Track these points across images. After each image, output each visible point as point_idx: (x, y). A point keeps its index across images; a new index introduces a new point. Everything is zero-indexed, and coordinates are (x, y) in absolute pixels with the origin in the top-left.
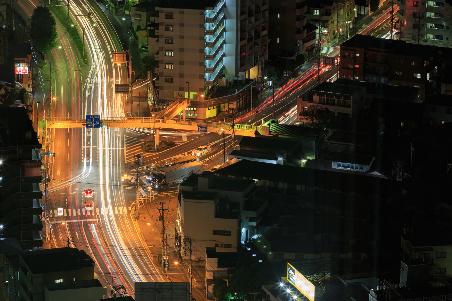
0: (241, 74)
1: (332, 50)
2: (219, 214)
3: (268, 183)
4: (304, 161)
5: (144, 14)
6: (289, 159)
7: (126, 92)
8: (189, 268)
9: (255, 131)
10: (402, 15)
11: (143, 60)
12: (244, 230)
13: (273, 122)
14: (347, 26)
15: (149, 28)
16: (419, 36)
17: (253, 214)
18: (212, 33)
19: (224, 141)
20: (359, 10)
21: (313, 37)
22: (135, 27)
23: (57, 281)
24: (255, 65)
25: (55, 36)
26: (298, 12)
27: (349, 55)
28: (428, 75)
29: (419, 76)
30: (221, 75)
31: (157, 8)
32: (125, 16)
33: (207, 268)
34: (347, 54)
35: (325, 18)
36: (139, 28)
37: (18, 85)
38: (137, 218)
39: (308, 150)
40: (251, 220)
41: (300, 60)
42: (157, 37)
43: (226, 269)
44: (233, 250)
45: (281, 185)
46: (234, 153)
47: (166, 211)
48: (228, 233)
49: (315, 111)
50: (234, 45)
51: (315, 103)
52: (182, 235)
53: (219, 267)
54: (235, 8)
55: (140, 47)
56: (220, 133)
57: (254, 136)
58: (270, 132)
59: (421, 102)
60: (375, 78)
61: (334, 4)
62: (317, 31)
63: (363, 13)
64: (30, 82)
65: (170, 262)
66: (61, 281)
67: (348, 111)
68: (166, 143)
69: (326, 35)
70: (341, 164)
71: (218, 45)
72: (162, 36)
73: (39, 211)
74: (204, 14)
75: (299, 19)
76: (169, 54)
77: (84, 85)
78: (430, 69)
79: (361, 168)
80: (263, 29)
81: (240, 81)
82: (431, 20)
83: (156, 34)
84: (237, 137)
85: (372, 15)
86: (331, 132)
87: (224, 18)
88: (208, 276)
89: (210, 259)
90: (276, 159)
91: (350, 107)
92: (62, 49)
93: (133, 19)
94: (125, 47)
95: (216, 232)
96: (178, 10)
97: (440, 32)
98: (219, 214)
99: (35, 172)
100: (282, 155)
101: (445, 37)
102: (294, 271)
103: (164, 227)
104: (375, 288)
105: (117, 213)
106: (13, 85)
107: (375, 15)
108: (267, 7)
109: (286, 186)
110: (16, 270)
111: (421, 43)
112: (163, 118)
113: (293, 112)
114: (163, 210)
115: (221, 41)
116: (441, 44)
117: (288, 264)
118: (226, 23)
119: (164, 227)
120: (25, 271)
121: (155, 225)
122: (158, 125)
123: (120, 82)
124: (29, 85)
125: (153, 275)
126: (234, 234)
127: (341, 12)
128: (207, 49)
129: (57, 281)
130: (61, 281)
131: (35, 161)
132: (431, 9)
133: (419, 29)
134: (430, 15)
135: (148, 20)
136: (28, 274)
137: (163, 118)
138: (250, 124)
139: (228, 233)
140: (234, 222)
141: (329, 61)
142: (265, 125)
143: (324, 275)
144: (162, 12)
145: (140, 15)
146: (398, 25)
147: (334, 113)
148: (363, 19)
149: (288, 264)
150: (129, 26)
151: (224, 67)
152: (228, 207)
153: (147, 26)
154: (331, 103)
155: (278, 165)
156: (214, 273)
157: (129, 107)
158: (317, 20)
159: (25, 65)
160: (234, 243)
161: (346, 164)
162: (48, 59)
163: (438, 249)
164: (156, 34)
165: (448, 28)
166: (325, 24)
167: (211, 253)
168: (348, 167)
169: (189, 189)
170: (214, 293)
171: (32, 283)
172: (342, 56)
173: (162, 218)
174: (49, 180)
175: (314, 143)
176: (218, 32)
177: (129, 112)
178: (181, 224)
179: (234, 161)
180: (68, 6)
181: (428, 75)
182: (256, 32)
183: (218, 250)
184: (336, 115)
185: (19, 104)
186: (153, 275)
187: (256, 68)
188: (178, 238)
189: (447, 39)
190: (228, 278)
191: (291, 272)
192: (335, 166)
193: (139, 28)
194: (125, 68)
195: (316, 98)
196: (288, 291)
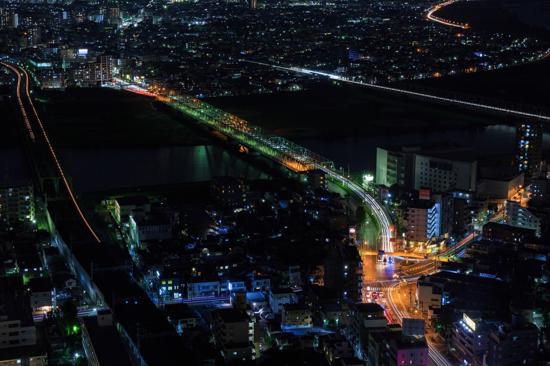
0: (441, 236)
1: (478, 228)
2: (434, 292)
3: (453, 281)
4: (468, 272)
5: (401, 210)
6: (462, 271)
7: (395, 241)
8: (422, 314)
9: (447, 259)
10: (508, 214)
11: (401, 229)
12: (443, 299)
13: (455, 256)
14: (485, 218)
15: (403, 216)
16: (516, 224)
17: (448, 293)
18: (431, 219)
19: (435, 262)
20: (490, 212)
21: (471, 222)
22: (397, 215)
23: (369, 316)
24: (447, 233)
25: (366, 218)
26: (465, 212)
27: (486, 230)
28: (519, 239)
29: (515, 240)
30: (433, 236)
31: (408, 208)
32: (394, 211)
33: (429, 314)
34: (485, 229)
35: (476, 214)
36: (399, 216)
37: (351, 237)
38: (399, 292)
39: (470, 268)
40: (447, 295)
41: (466, 231)
42: (408, 220)
43: (436, 315)
44: (439, 307)
45: (459, 282)
46: (439, 268)
47: (412, 290)
48: (437, 300)
49: (472, 252)
50: (439, 224)
51: (472, 249)
52: (418, 300)
53: (434, 314)
54: (440, 209)
55: (399, 223)
56: (433, 260)
57: (447, 261)
58: (454, 260)
59: (517, 250)
60: (497, 240)
61: (480, 209)
62: (473, 220)
63: (491, 213)
64: (356, 236)
65: (413, 311)
66: (371, 316)
67: (486, 253)
68: (410, 262)
69: (476, 221)
70: (484, 274)
71: (433, 224)
72: (410, 219)
73: (361, 288)
74: (427, 211)
75: (465, 214)
76: (412, 227)
77: (377, 237)
78: (520, 237)
79: (492, 276)
80: (451, 218)
81: (441, 239)
82: (520, 217)
83: (408, 218)
84: (440, 262)
85: (495, 214)
86: (479, 262)
87: (435, 213)
88: (429, 317)
89: (430, 310)
90: (457, 271)
91: (487, 251)
92: (57, 306)
93: (397, 212)
94: (394, 224)
95: (432, 300)
96: (417, 209)
97: (524, 222)
98: (434, 292)
99: (360, 272)
100: (459, 270)
101: (526, 224)
102: (466, 317)
103: (411, 296)
104: (501, 326)
105: (385, 290)
106: (349, 237)
107: (496, 214)
108: (452, 209)
109: (461, 282)
110: (352, 311)
111: (516, 226)
112: (410, 252)
113: (463, 252)
114: (411, 289)
115: (434, 222)
116: (525, 227)
117: (464, 314)
118: (436, 215)
119: (411, 296)
120: (356, 312)
121: (407, 296)
122: (408, 255)
123: (391, 237)
124: (355, 237)
125: (406, 316)
126: (440, 301)
127: (482, 212)
128: (428, 225)
129: (369, 316)
130: (371, 316)
131: (360, 267)
132: (520, 212)
133: (515, 220)
134: (520, 215)
135: (403, 213)
136: (357, 313)
137: (410, 252)
138: (445, 256)
139: (437, 300)
140: (440, 296)
141: (478, 232)
142: (452, 257)
143: (479, 319)
144: (410, 209)
145: (400, 211)
146: (506, 219)
147: (480, 253)
148: (491, 215)
149: (464, 314)
150: (395, 215)
151: (435, 233)
152: (437, 289)
153: (402, 215)
154: (479, 249)
155: (457, 273)
156: (432, 316)
157: (395, 247)
158: (473, 215)
159: (354, 229)
160: (440, 305)
161: (486, 274)
162: (363, 227)
163: (526, 311)
164: (408, 218)
165: (527, 220)
166: (476, 217)
167: (431, 308)
168: (486, 275)
169: (422, 281)
170: (432, 325)
171: (359, 316)
172: (483, 230)
173: (410, 293)
174: (364, 275)
175: (472, 265)
176: (433, 219)
177: (395, 249)
178: (418, 296)
179: (439, 271)
180: (371, 206)
181: (519, 239)
182: (448, 219)
183: (433, 307)
184: (481, 254)
185: (351, 244)
186: (406, 316)
187: (447, 234)
188: (416, 301)
189: (527, 225)
190: (437, 319)
191: (465, 317)
192: (481, 275)
193: (399, 216)
194: (393, 233)
195: (473, 247)
196: (464, 325)
